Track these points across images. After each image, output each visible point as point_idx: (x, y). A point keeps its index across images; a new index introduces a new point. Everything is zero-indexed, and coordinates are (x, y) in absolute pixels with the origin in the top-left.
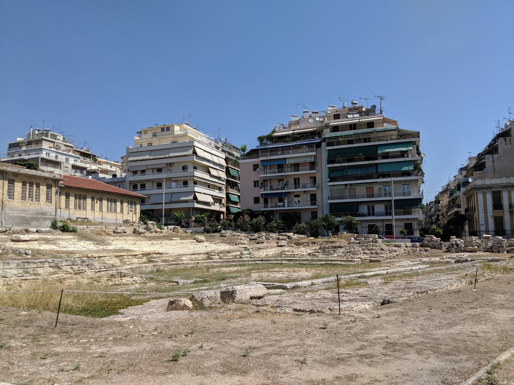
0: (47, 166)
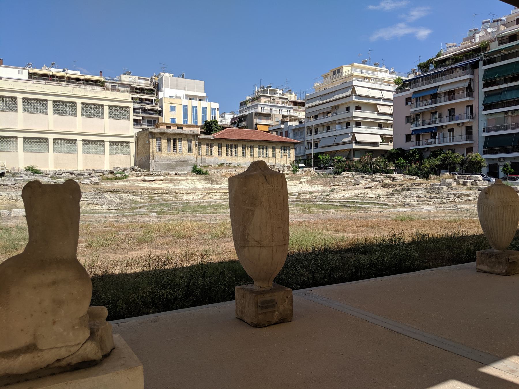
0: (260, 119)
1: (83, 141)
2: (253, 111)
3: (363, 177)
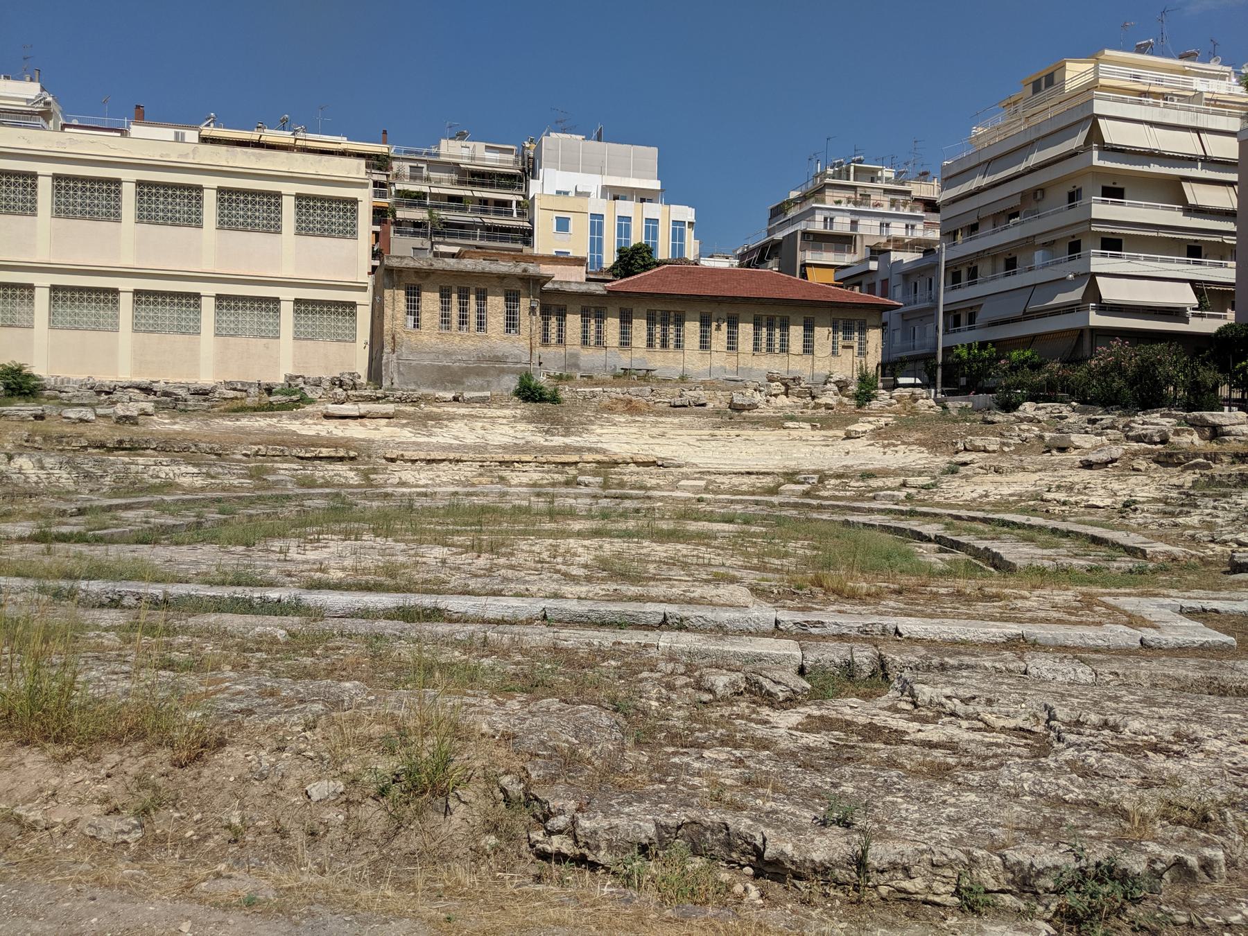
0: (819, 249)
1: (219, 297)
2: (801, 226)
3: (1093, 422)
